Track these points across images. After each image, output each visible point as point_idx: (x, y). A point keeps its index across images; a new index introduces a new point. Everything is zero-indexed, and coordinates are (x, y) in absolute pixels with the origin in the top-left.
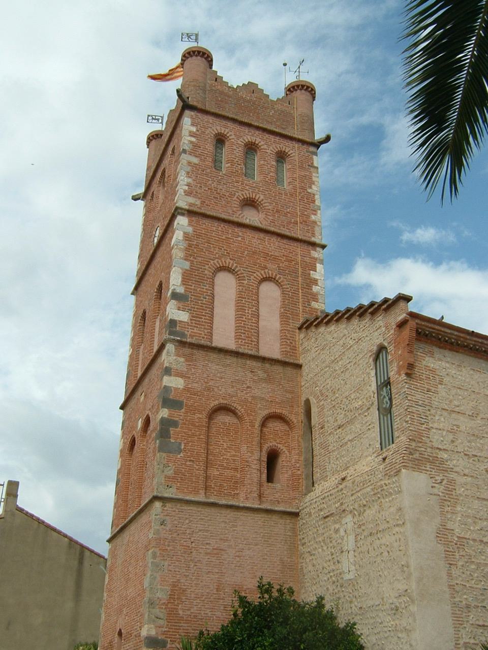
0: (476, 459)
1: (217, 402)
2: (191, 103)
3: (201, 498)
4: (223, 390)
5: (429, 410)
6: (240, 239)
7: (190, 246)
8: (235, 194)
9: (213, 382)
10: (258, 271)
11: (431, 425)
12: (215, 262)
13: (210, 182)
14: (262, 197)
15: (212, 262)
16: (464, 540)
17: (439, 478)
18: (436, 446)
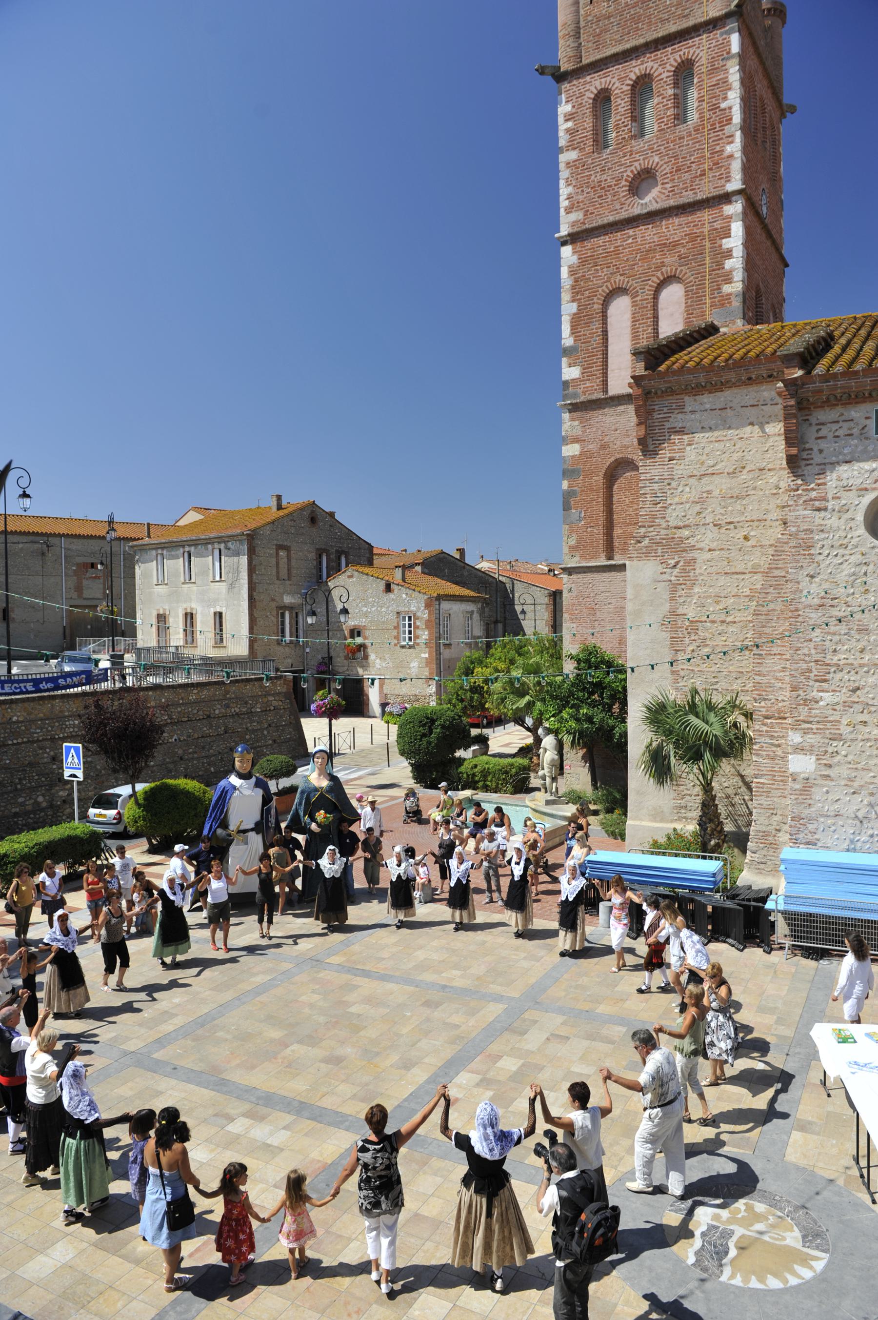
0: (731, 526)
1: (613, 459)
2: (138, 571)
3: (602, 561)
4: (618, 443)
5: (669, 484)
6: (630, 241)
7: (576, 281)
8: (622, 176)
9: (608, 437)
10: (653, 275)
11: (669, 502)
12: (604, 287)
13: (593, 177)
14: (657, 159)
15: (600, 289)
16: (700, 624)
17: (672, 562)
18: (674, 525)
